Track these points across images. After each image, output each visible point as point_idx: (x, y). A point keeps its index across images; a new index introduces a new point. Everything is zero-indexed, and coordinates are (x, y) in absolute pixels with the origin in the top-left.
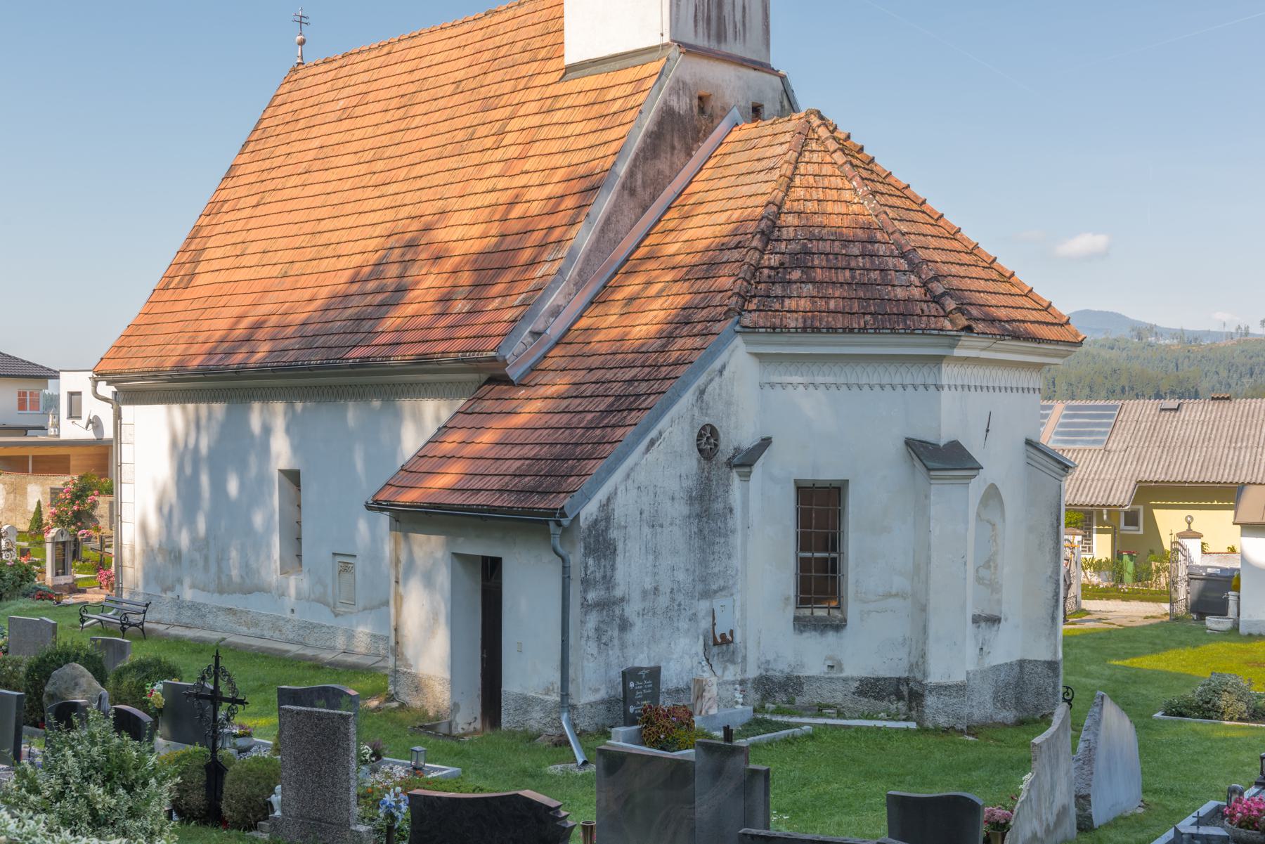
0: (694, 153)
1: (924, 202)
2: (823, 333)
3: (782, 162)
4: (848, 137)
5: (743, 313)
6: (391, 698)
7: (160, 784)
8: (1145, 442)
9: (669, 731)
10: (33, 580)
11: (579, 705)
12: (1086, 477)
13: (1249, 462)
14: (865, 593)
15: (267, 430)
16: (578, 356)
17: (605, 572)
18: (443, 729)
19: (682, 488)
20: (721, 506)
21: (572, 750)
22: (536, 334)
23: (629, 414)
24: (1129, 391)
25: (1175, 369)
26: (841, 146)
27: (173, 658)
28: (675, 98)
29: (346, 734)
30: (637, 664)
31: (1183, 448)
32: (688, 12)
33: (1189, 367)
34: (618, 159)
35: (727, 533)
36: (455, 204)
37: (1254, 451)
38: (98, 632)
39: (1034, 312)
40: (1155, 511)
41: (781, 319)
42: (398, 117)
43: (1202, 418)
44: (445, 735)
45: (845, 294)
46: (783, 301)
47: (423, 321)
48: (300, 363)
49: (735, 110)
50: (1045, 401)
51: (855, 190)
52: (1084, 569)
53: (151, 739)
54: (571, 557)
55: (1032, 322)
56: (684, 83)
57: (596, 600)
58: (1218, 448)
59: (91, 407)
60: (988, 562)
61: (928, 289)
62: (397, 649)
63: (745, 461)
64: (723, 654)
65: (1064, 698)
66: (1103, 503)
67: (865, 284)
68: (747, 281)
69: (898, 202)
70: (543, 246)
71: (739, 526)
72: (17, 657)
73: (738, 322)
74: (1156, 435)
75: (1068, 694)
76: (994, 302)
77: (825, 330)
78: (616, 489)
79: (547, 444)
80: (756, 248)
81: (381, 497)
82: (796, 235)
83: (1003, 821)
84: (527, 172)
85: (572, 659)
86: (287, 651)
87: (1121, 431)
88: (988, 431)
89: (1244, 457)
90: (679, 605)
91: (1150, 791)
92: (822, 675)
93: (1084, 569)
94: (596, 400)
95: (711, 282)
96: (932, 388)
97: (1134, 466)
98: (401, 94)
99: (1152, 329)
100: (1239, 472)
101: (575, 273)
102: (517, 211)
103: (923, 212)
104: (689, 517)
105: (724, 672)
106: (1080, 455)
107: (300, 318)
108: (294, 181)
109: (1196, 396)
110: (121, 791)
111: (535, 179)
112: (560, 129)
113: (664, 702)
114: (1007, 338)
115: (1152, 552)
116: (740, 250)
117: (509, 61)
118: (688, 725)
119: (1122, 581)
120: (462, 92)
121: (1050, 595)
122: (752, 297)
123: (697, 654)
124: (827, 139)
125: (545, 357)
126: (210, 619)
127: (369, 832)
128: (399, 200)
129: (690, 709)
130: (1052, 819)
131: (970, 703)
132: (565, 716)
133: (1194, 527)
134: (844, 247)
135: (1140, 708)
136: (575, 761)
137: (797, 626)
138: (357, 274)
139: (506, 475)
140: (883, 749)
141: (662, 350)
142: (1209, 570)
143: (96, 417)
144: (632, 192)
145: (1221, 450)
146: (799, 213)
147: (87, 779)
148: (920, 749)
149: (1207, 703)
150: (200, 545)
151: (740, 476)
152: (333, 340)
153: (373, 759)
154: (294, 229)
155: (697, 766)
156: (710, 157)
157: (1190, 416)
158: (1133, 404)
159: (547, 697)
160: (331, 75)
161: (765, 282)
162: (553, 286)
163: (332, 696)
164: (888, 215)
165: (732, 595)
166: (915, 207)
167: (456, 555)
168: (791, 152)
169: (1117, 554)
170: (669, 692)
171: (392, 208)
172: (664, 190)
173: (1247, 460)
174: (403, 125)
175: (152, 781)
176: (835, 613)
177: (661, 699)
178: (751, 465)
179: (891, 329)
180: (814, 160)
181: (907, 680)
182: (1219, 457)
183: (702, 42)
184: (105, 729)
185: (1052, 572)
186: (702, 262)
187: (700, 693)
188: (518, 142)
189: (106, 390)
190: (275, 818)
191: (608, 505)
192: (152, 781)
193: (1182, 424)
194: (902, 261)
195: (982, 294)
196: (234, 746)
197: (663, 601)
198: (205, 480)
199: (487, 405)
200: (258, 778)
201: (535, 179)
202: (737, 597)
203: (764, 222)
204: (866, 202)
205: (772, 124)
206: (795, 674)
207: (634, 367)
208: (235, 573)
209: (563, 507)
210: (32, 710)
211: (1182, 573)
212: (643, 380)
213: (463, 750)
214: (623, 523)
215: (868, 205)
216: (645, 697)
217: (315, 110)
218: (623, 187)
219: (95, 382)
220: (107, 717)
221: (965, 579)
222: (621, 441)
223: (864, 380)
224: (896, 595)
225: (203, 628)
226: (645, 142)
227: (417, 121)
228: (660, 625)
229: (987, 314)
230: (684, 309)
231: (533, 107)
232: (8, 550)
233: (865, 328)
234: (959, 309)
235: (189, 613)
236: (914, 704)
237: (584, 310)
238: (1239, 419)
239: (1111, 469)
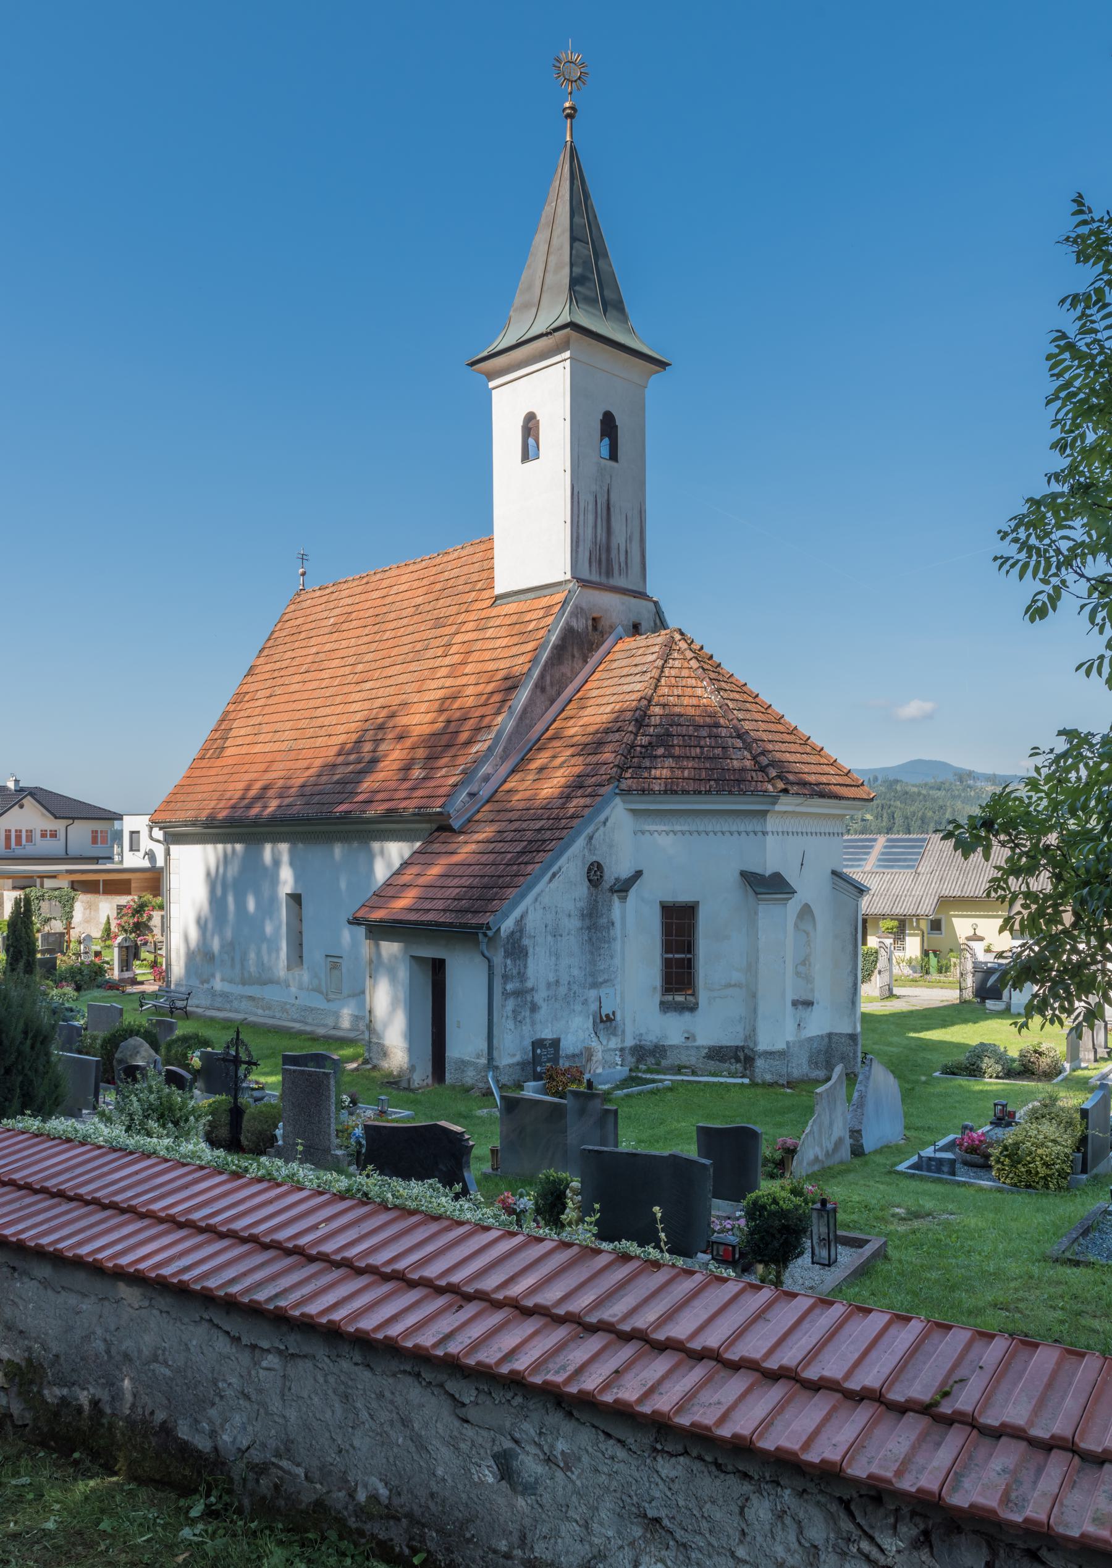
1: (757, 696)
4: (702, 648)
6: (366, 1062)
7: (197, 1120)
10: (104, 976)
11: (501, 1066)
15: (277, 863)
18: (404, 1084)
19: (576, 907)
20: (605, 921)
22: (472, 795)
27: (206, 1033)
28: (575, 621)
29: (328, 1086)
30: (543, 1036)
32: (584, 556)
35: (609, 941)
36: (416, 698)
38: (153, 1014)
40: (954, 920)
53: (191, 1090)
55: (835, 785)
56: (582, 609)
59: (145, 844)
62: (370, 1027)
63: (623, 888)
64: (607, 1029)
69: (737, 696)
70: (478, 730)
71: (619, 936)
72: (95, 1033)
73: (617, 787)
76: (806, 770)
80: (631, 732)
81: (358, 915)
83: (792, 1148)
85: (495, 1032)
86: (293, 1028)
90: (575, 993)
95: (598, 756)
99: (970, 774)
103: (756, 703)
104: (582, 929)
107: (300, 781)
108: (298, 678)
110: (170, 1125)
117: (455, 591)
119: (927, 973)
121: (850, 985)
122: (627, 768)
123: (588, 1028)
124: (685, 650)
126: (235, 1004)
127: (344, 1155)
128: (374, 693)
129: (582, 1069)
130: (830, 1147)
134: (696, 730)
138: (342, 749)
140: (722, 1098)
141: (562, 807)
143: (151, 850)
144: (543, 690)
146: (664, 705)
147: (147, 1117)
148: (750, 1098)
149: (973, 1065)
150: (229, 947)
152: (326, 799)
159: (478, 1061)
160: (324, 599)
163: (319, 1059)
166: (750, 699)
167: (414, 958)
169: (925, 953)
170: (567, 1057)
175: (192, 1118)
176: (690, 998)
177: (561, 1062)
178: (627, 891)
180: (676, 666)
181: (743, 1048)
183: (595, 578)
184: (160, 1082)
189: (158, 834)
190: (279, 1146)
192: (192, 1118)
196: (252, 1096)
197: (563, 990)
198: (230, 899)
199: (436, 847)
202: (618, 987)
203: (638, 712)
208: (253, 969)
210: (105, 1071)
211: (969, 966)
217: (313, 625)
219: (151, 828)
220: (160, 1074)
223: (709, 828)
224: (735, 985)
225: (230, 1011)
229: (801, 779)
230: (578, 776)
232: (86, 953)
233: (710, 791)
235: (220, 1000)
237: (508, 777)
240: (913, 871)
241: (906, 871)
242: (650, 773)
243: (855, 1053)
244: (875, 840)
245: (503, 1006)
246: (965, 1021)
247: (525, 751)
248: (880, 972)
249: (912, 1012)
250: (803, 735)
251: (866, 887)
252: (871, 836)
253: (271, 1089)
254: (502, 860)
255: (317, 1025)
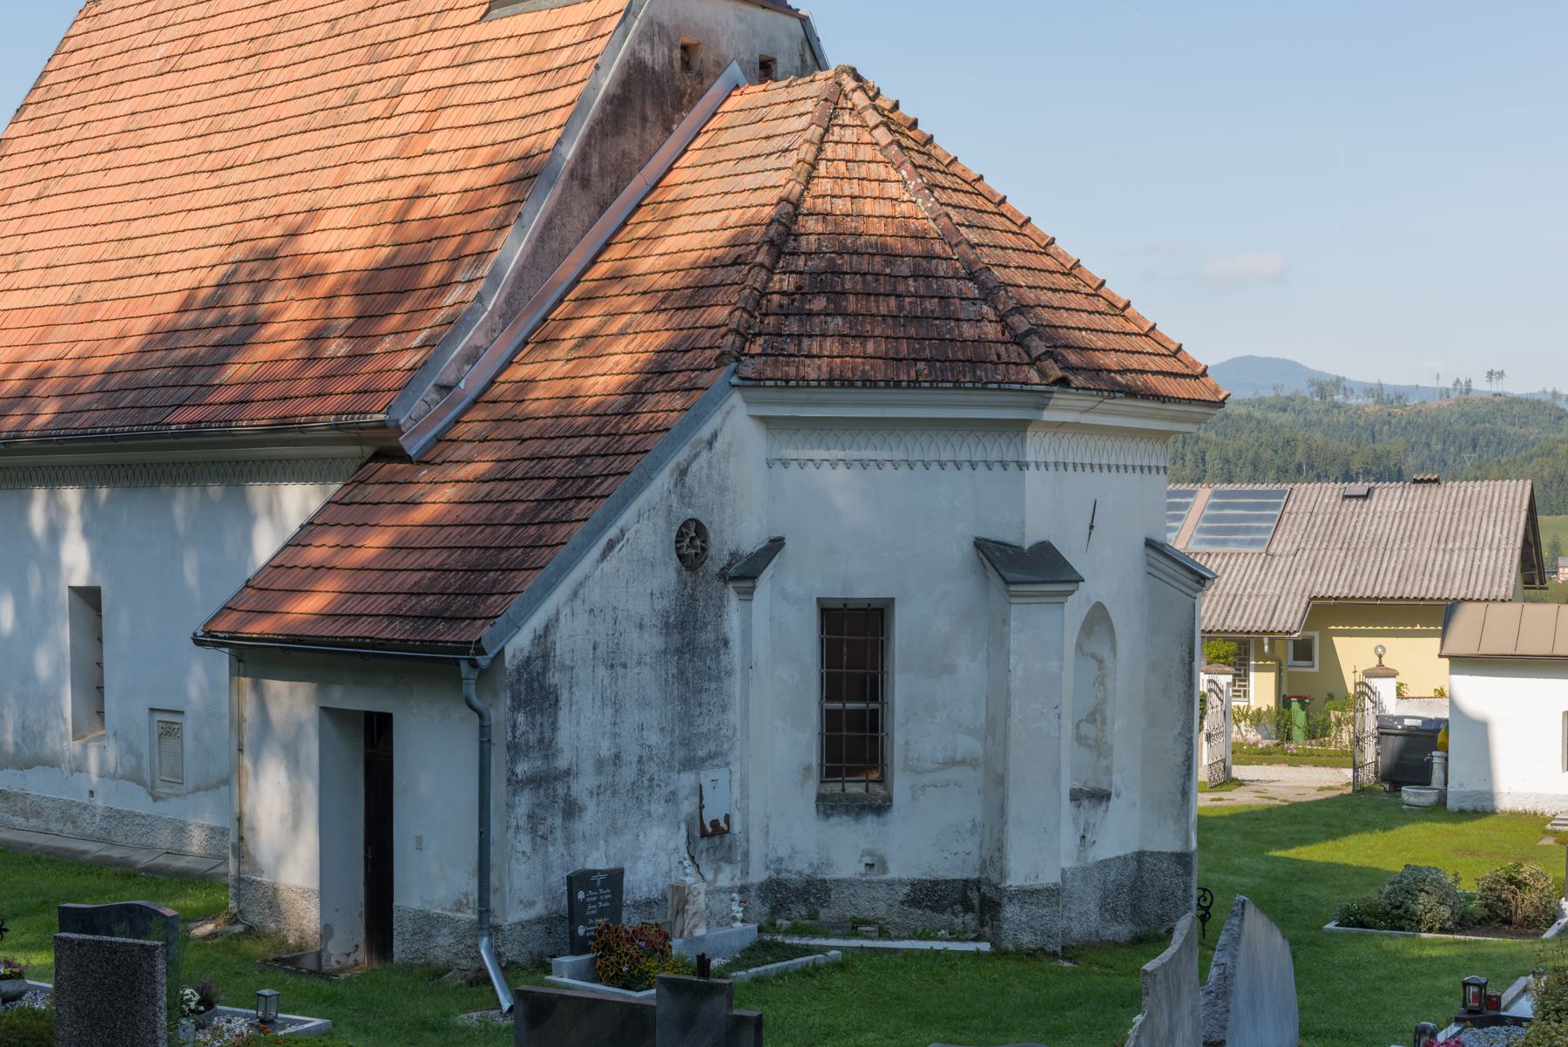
0: (675, 127)
1: (1003, 200)
2: (881, 388)
3: (801, 141)
4: (896, 106)
5: (743, 358)
6: (234, 920)
8: (1321, 543)
9: (635, 961)
11: (505, 926)
12: (1240, 592)
13: (1463, 570)
14: (918, 760)
15: (55, 533)
16: (506, 420)
17: (542, 733)
18: (309, 963)
20: (712, 636)
21: (494, 990)
22: (444, 388)
23: (578, 504)
24: (1307, 471)
25: (1371, 440)
26: (885, 119)
28: (647, 48)
29: (151, 973)
30: (589, 866)
31: (1374, 551)
33: (1390, 437)
34: (564, 134)
35: (720, 676)
37: (1471, 555)
39: (1157, 358)
40: (1336, 640)
41: (797, 368)
42: (246, 71)
43: (1400, 509)
44: (310, 972)
45: (889, 332)
46: (800, 343)
47: (284, 368)
48: (99, 430)
49: (735, 67)
50: (1224, 485)
51: (904, 182)
52: (1237, 722)
54: (492, 713)
55: (1154, 373)
56: (661, 26)
57: (528, 773)
58: (1422, 550)
60: (1093, 713)
61: (1007, 324)
62: (241, 849)
64: (715, 849)
65: (1199, 905)
66: (1264, 628)
67: (918, 317)
68: (749, 313)
69: (965, 200)
71: (738, 666)
73: (735, 372)
74: (1337, 531)
75: (1205, 900)
76: (1100, 344)
77: (859, 384)
78: (558, 613)
79: (458, 548)
80: (762, 265)
82: (820, 245)
84: (432, 153)
85: (494, 859)
86: (84, 852)
87: (1288, 527)
88: (1091, 527)
89: (1457, 563)
90: (651, 779)
91: (1312, 1034)
92: (858, 877)
93: (1237, 722)
94: (530, 484)
96: (1013, 467)
97: (1306, 576)
98: (250, 36)
99: (1338, 383)
100: (1449, 584)
101: (502, 299)
102: (421, 209)
103: (1002, 215)
104: (665, 652)
105: (716, 875)
106: (1232, 562)
107: (105, 364)
109: (1398, 476)
111: (445, 162)
112: (481, 91)
113: (629, 919)
114: (1118, 395)
115: (1331, 697)
116: (740, 268)
118: (662, 952)
119: (1289, 738)
120: (338, 35)
121: (1180, 760)
122: (755, 335)
123: (677, 849)
124: (865, 108)
125: (457, 422)
129: (666, 929)
131: (1066, 914)
132: (484, 942)
133: (1386, 662)
134: (889, 264)
135: (1307, 917)
136: (499, 1006)
137: (821, 808)
139: (398, 593)
140: (941, 981)
141: (627, 412)
142: (1407, 722)
144: (585, 183)
145: (1426, 552)
146: (825, 215)
148: (995, 981)
149: (1398, 907)
151: (739, 593)
153: (202, 1008)
154: (92, 234)
155: (658, 1012)
156: (698, 134)
157: (1384, 505)
158: (1306, 489)
161: (774, 314)
162: (468, 318)
163: (137, 918)
164: (951, 219)
165: (727, 764)
166: (991, 207)
168: (813, 127)
169: (1284, 701)
170: (637, 905)
171: (236, 203)
172: (631, 180)
173: (1461, 567)
174: (253, 82)
176: (877, 789)
177: (625, 915)
179: (955, 382)
180: (847, 139)
181: (977, 883)
182: (1423, 563)
185: (1183, 727)
186: (684, 284)
187: (681, 907)
188: (419, 109)
191: (545, 636)
193: (1373, 517)
194: (971, 284)
195: (1084, 333)
197: (628, 774)
199: (372, 492)
200: (24, 1039)
201: (445, 162)
202: (735, 767)
203: (775, 226)
204: (920, 201)
205: (787, 87)
206: (820, 876)
207: (585, 436)
209: (480, 640)
211: (1371, 725)
212: (598, 455)
213: (336, 993)
214: (568, 662)
215: (923, 204)
216: (601, 913)
217: (125, 59)
218: (572, 175)
221: (1059, 738)
222: (564, 543)
224: (963, 762)
226: (603, 110)
227: (274, 76)
228: (622, 809)
231: (442, 58)
233: (917, 381)
234: (1049, 354)
236: (987, 917)
238: (1450, 510)
239: (1274, 581)
240: (1263, 549)
241: (1250, 550)
242: (799, 345)
243: (1187, 889)
244: (1192, 494)
245: (510, 806)
246: (1368, 826)
247: (549, 304)
248: (1209, 737)
249: (1270, 810)
250: (1092, 277)
251: (1209, 571)
252: (1184, 487)
253: (38, 977)
254: (507, 517)
255: (134, 848)
